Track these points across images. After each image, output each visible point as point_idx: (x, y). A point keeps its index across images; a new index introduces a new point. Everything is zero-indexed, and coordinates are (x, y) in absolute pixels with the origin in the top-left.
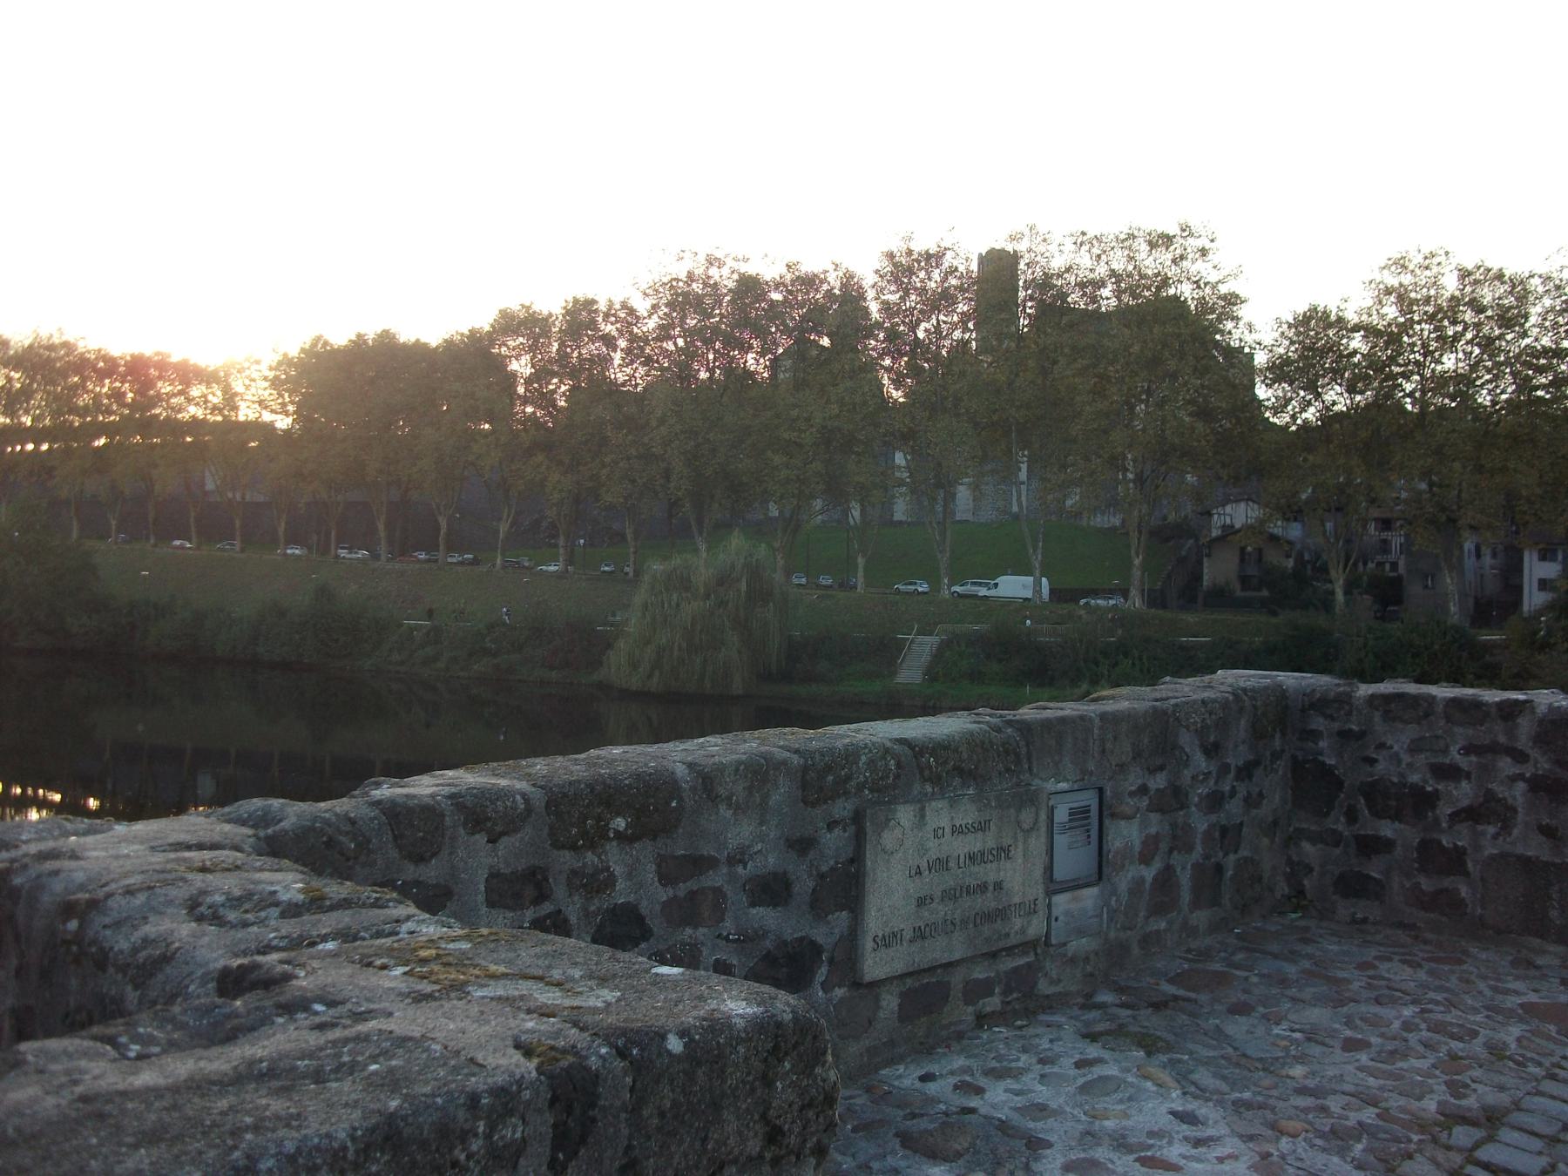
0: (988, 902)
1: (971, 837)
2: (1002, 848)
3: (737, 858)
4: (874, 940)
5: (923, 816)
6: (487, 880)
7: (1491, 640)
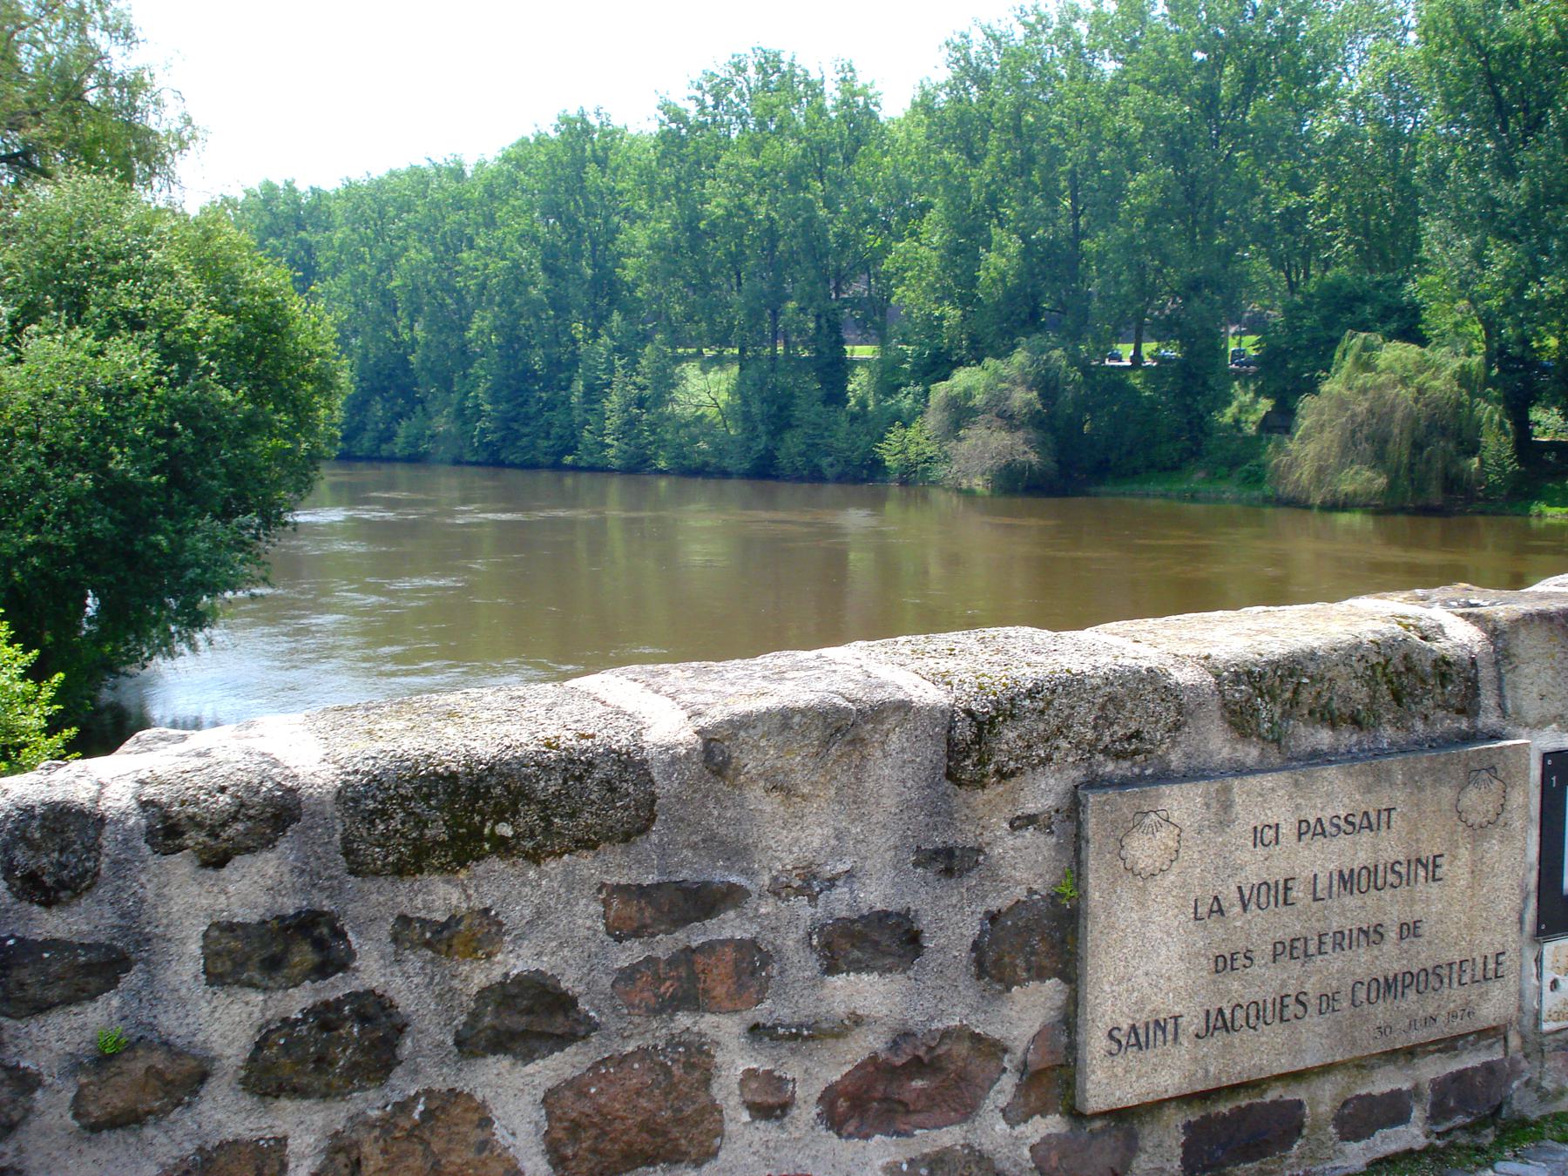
0: (1389, 959)
1: (1343, 841)
2: (1419, 861)
3: (809, 882)
4: (1111, 1036)
5: (1227, 806)
6: (205, 935)
7: (437, 577)
